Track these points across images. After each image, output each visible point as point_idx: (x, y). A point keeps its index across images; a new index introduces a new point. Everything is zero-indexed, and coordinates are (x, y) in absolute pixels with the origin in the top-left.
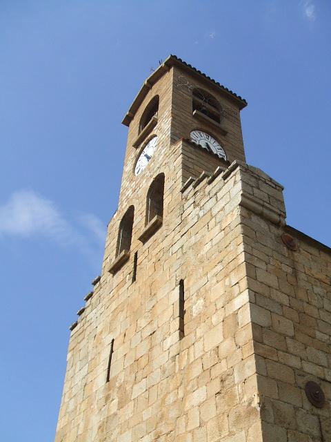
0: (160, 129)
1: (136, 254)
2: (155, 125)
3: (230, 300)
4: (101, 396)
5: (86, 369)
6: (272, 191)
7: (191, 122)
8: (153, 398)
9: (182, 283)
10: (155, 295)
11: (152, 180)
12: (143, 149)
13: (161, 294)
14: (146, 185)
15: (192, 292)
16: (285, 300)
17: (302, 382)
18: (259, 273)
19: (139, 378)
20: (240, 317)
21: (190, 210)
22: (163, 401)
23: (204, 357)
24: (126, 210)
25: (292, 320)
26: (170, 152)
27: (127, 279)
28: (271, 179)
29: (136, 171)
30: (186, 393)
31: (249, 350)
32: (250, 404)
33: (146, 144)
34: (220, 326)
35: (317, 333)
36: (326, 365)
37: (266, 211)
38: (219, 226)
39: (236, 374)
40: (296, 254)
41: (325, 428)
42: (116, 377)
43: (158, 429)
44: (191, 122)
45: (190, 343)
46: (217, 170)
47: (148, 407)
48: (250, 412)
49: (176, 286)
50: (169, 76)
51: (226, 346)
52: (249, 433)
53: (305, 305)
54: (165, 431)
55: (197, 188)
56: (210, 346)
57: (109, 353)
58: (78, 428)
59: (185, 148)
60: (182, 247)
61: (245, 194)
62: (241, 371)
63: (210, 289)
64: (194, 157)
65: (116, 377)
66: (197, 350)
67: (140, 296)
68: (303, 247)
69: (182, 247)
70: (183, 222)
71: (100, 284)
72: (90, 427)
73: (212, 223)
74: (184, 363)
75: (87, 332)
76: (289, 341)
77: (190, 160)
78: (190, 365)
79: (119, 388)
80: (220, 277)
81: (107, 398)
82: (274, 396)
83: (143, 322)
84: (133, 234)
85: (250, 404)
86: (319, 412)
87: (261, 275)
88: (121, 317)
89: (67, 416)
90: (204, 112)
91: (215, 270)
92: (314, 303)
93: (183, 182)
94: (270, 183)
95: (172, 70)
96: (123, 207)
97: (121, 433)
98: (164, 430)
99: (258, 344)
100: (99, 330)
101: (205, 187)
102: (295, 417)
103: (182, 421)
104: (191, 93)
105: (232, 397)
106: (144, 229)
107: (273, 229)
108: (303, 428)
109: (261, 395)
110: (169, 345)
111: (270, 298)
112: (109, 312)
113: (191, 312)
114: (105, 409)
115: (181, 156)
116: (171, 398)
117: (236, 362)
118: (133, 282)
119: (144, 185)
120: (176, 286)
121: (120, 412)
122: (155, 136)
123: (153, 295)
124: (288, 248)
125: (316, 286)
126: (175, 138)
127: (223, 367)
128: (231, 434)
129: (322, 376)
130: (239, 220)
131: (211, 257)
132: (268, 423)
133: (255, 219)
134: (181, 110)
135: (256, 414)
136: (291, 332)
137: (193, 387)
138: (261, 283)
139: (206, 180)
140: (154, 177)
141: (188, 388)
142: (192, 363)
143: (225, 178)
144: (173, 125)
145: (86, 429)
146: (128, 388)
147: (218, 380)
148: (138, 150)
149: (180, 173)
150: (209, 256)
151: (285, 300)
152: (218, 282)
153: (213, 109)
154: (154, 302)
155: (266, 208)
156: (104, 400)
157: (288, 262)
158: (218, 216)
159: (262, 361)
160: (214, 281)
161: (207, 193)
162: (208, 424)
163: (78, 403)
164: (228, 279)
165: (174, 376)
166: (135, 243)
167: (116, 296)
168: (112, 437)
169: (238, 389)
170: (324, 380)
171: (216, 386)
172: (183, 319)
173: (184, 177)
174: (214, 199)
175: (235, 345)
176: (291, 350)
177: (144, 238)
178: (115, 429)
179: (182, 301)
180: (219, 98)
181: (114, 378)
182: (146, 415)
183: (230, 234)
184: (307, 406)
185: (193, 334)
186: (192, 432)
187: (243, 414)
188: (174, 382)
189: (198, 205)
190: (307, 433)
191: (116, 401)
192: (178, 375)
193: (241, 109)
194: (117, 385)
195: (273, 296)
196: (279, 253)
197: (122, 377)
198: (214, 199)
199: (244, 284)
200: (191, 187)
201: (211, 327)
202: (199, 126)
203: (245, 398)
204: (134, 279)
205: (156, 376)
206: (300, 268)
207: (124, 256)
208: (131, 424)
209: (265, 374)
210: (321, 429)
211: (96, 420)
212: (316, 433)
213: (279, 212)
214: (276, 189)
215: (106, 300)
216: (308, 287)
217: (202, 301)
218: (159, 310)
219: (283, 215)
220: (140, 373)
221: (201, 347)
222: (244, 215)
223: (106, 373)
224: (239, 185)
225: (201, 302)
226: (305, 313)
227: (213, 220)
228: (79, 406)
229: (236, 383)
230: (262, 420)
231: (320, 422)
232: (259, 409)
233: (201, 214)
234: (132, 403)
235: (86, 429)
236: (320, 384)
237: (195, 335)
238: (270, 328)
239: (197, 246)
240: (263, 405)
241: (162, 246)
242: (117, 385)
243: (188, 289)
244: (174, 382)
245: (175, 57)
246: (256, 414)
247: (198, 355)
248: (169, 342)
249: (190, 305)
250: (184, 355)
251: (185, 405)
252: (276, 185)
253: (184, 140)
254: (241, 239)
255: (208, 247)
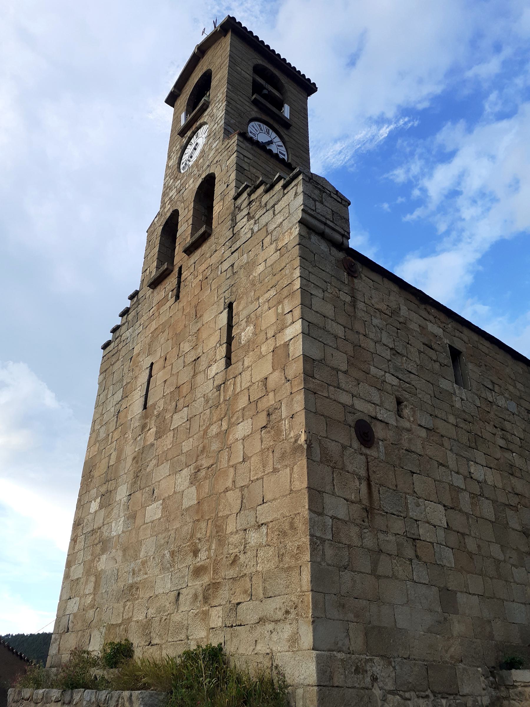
0: (212, 116)
1: (180, 268)
2: (206, 110)
3: (282, 329)
4: (137, 424)
5: (119, 395)
6: (336, 207)
7: (249, 109)
8: (195, 427)
9: (230, 306)
10: (200, 317)
11: (200, 180)
12: (190, 138)
13: (207, 317)
14: (193, 185)
15: (241, 317)
16: (340, 331)
17: (351, 419)
18: (314, 301)
19: (180, 406)
20: (291, 348)
21: (243, 224)
22: (205, 432)
23: (251, 389)
24: (168, 215)
25: (345, 353)
26: (223, 146)
27: (170, 296)
28: (337, 191)
29: (182, 166)
30: (231, 425)
31: (299, 385)
32: (296, 441)
33: (194, 133)
34: (270, 357)
35: (372, 369)
36: (378, 402)
37: (328, 231)
38: (274, 245)
39: (283, 408)
40: (356, 281)
41: (372, 469)
42: (154, 405)
43: (199, 463)
44: (249, 109)
45: (237, 372)
46: (276, 177)
47: (189, 438)
48: (296, 449)
49: (225, 309)
50: (227, 41)
51: (276, 378)
52: (294, 470)
53: (361, 337)
54: (206, 465)
55: (253, 197)
56: (258, 377)
57: (147, 378)
58: (110, 459)
59: (240, 143)
60: (232, 266)
61: (307, 209)
62: (290, 404)
63: (261, 316)
64: (250, 156)
65: (154, 405)
66: (244, 381)
67: (184, 317)
68: (364, 272)
69: (232, 266)
70: (235, 236)
71: (138, 300)
72: (123, 457)
73: (267, 240)
74: (230, 392)
75: (123, 353)
76: (341, 375)
77: (246, 159)
78: (236, 396)
79: (158, 416)
80: (273, 303)
81: (143, 427)
82: (321, 434)
83: (186, 347)
84: (177, 244)
85: (296, 441)
86: (368, 451)
87: (317, 303)
88: (162, 338)
89: (98, 444)
90: (265, 96)
91: (267, 296)
92: (372, 335)
93: (237, 187)
94: (335, 196)
95: (229, 35)
96: (166, 210)
97: (157, 465)
98: (205, 462)
99: (309, 378)
100: (136, 351)
101: (261, 196)
102: (342, 456)
103: (225, 454)
104: (251, 69)
105: (279, 432)
106: (189, 240)
107: (334, 251)
108: (350, 468)
109: (308, 432)
110: (213, 373)
111: (324, 329)
112: (149, 332)
113: (240, 338)
114: (141, 439)
115: (235, 155)
116: (214, 430)
117: (285, 396)
118: (176, 301)
119: (191, 186)
120: (225, 309)
121: (157, 443)
122: (205, 123)
123: (197, 316)
124: (348, 274)
125: (375, 317)
126: (229, 129)
127: (270, 400)
128: (275, 470)
129: (373, 414)
130: (297, 241)
131: (264, 280)
132: (315, 462)
133: (315, 238)
134: (238, 93)
135: (302, 452)
136: (344, 367)
137: (238, 418)
138: (317, 312)
139: (262, 189)
140: (203, 176)
141: (233, 420)
142: (238, 393)
143: (285, 187)
144: (227, 113)
145: (119, 459)
146: (168, 416)
147: (265, 414)
148: (185, 140)
149: (233, 176)
150: (261, 278)
151: (340, 331)
152: (270, 308)
153: (277, 94)
154: (199, 325)
155: (329, 226)
156: (139, 429)
157: (346, 289)
158: (275, 233)
159: (311, 396)
160: (266, 307)
161: (263, 204)
162: (252, 459)
163: (111, 431)
164: (281, 306)
165: (218, 406)
166: (179, 256)
167: (156, 314)
168: (148, 470)
169: (285, 425)
170: (376, 418)
171: (262, 419)
172: (231, 345)
173: (238, 181)
174: (271, 212)
175: (284, 378)
176: (343, 385)
177: (189, 250)
178: (151, 460)
179: (230, 326)
180: (284, 80)
181: (151, 406)
182: (187, 446)
183: (287, 255)
184: (356, 444)
185: (241, 363)
186: (234, 467)
187: (288, 451)
188: (218, 412)
189: (253, 217)
190: (354, 473)
191: (154, 430)
192: (223, 406)
193: (309, 95)
194: (156, 413)
195: (328, 327)
196: (338, 280)
197: (161, 405)
198: (271, 212)
199: (297, 312)
200: (245, 195)
201: (261, 357)
202: (258, 116)
203: (292, 434)
204: (177, 297)
205: (199, 404)
206: (359, 296)
207: (167, 269)
208: (170, 456)
209: (314, 410)
210: (368, 470)
211: (130, 450)
212: (363, 473)
213: (343, 232)
214: (341, 203)
215: (145, 318)
216: (367, 318)
217: (252, 327)
218: (204, 335)
219: (346, 236)
220: (182, 400)
221: (249, 378)
222: (303, 234)
223: (143, 399)
224: (300, 199)
225: (250, 329)
226: (360, 346)
227: (269, 236)
228: (111, 434)
229: (283, 418)
230: (308, 458)
231: (368, 462)
232: (305, 446)
233: (256, 229)
234: (171, 433)
235: (119, 459)
236: (371, 422)
237: (243, 365)
238: (322, 361)
239: (251, 265)
240: (309, 442)
241: (210, 261)
242: (156, 413)
243: (238, 314)
244: (218, 412)
245: (234, 19)
246: (302, 452)
247: (245, 385)
248: (214, 370)
249: (239, 331)
250: (230, 384)
251: (228, 437)
252: (341, 199)
253: (240, 134)
254: (297, 262)
255: (261, 268)
